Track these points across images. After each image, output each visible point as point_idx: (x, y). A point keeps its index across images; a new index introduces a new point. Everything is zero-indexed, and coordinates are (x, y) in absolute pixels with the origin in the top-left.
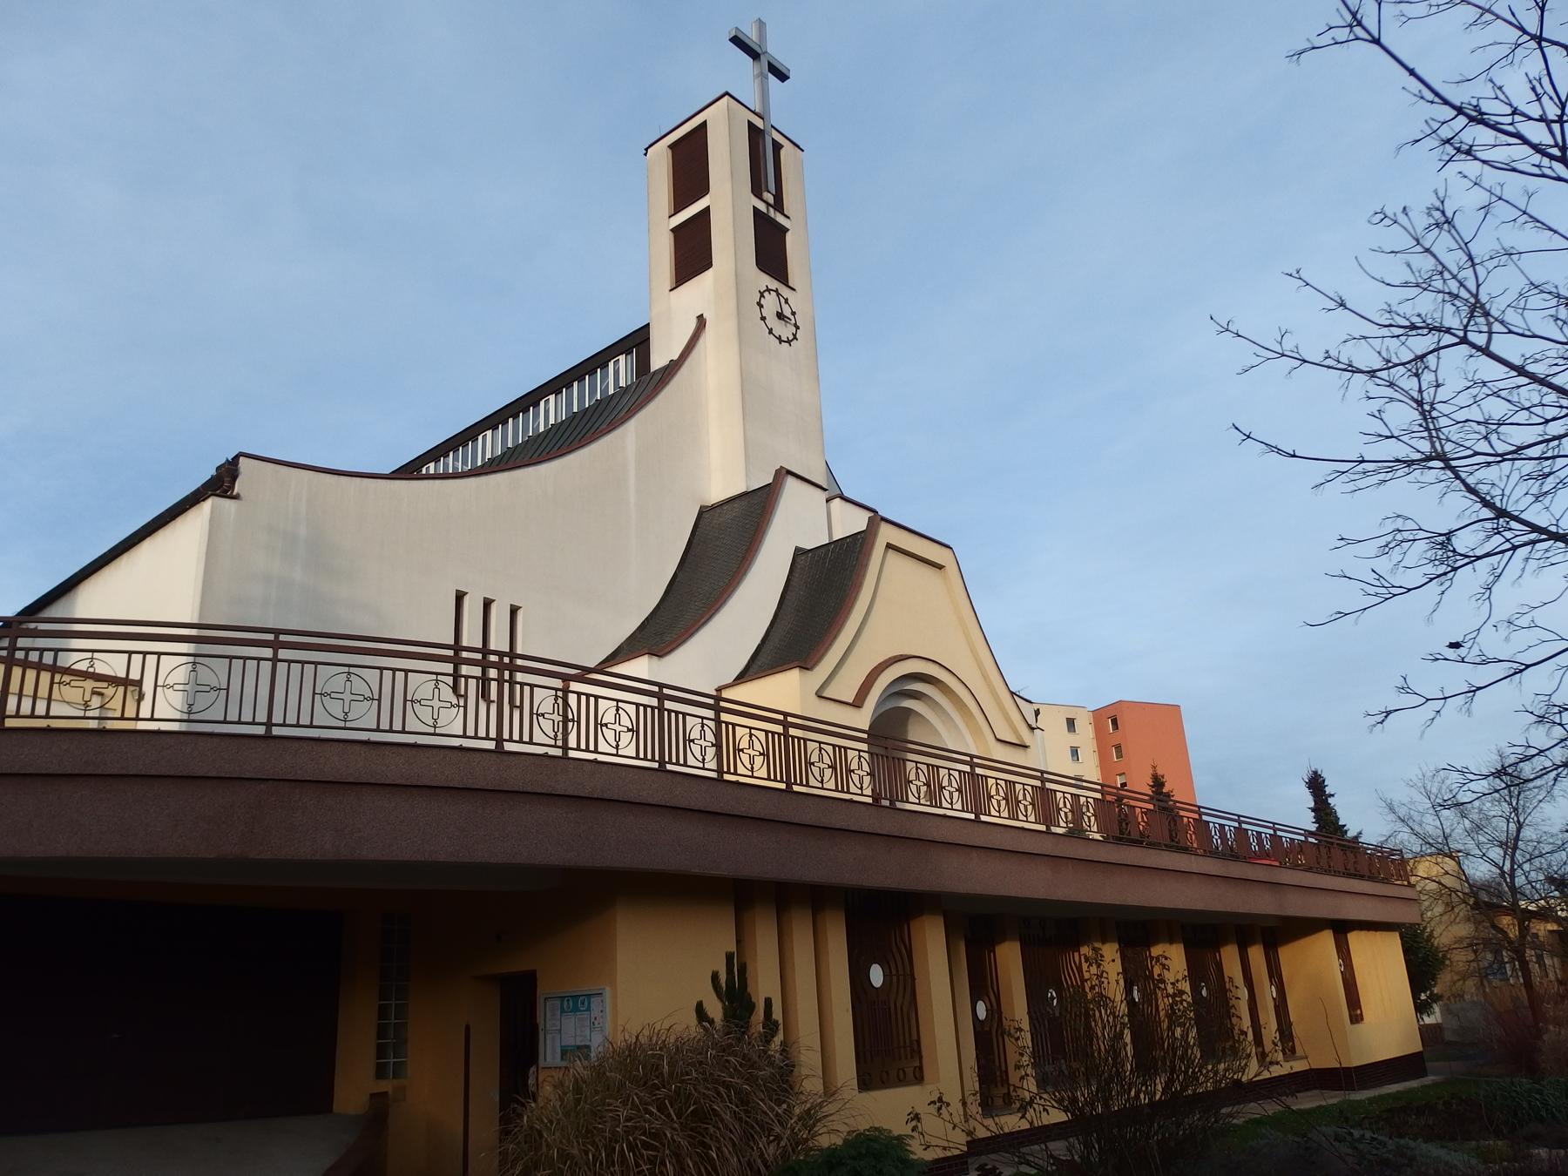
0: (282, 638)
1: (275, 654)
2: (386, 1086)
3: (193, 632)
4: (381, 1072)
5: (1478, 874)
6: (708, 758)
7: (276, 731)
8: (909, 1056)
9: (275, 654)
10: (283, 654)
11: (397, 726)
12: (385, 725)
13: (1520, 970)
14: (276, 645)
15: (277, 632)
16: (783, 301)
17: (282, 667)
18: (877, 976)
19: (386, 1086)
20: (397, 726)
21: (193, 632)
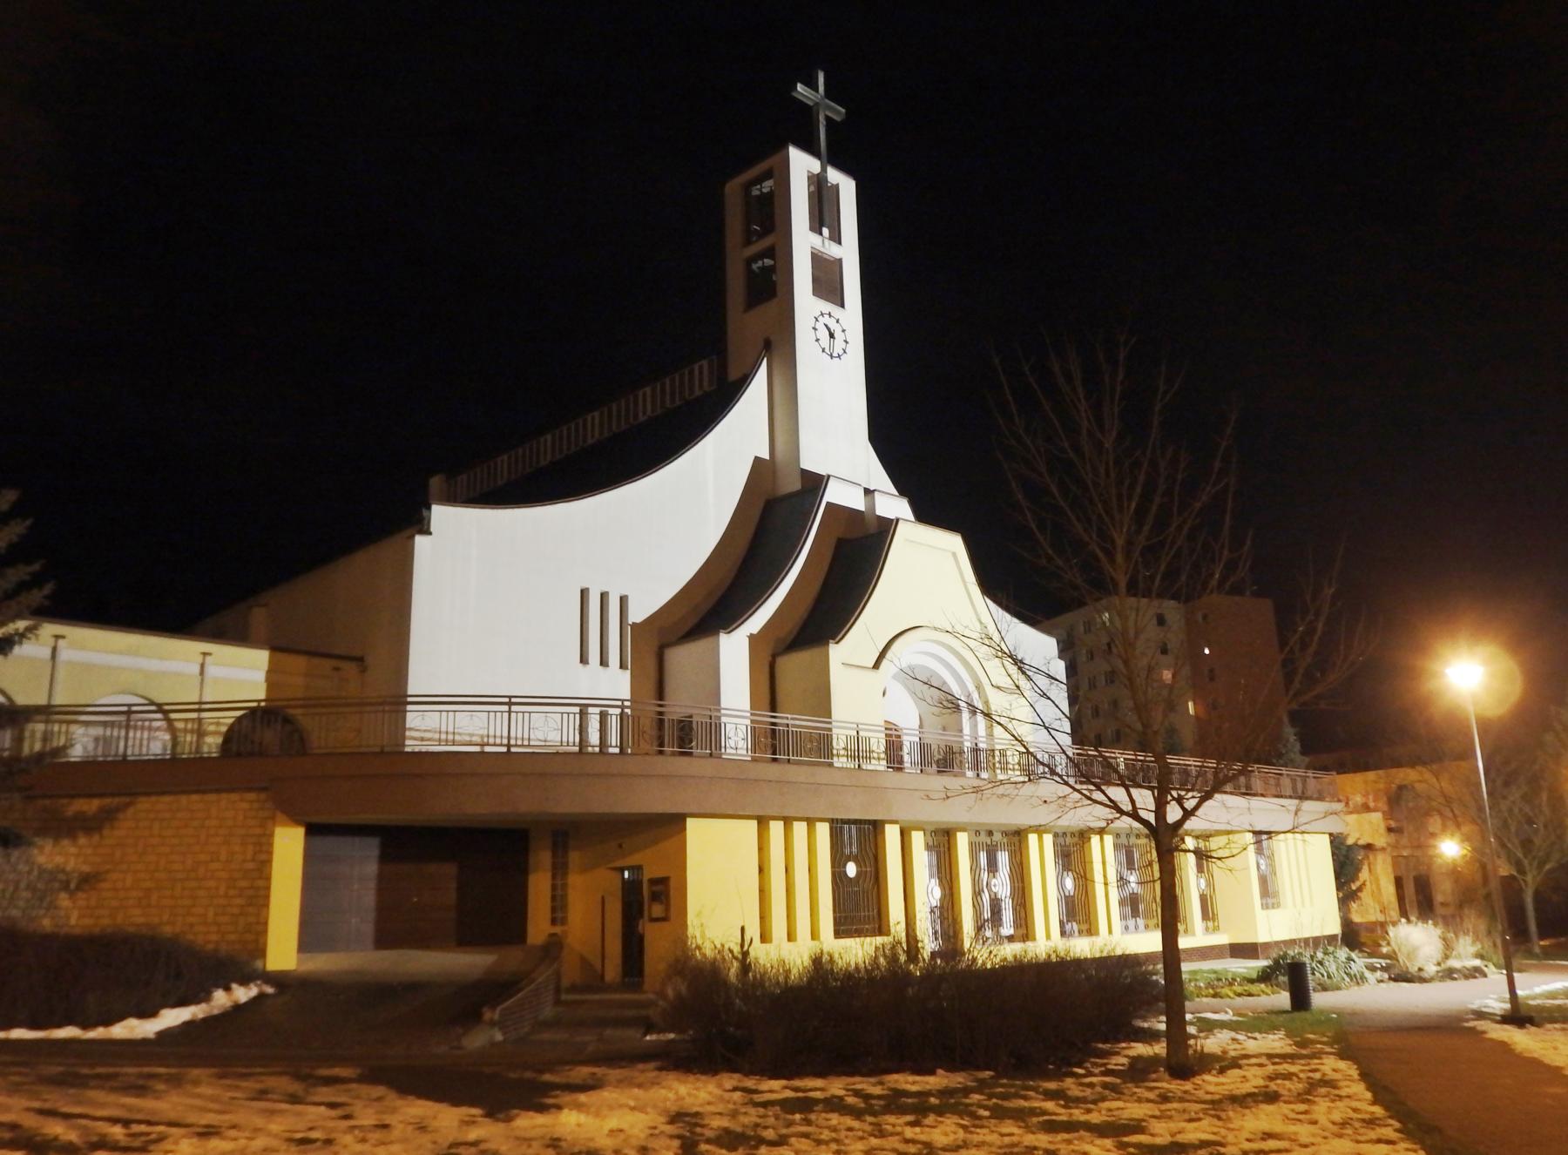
0: (513, 700)
1: (510, 708)
2: (558, 929)
3: (301, 702)
4: (554, 922)
5: (205, 1090)
6: (1106, 901)
7: (513, 750)
8: (888, 732)
9: (510, 708)
10: (514, 708)
11: (565, 716)
12: (527, 715)
13: (205, 997)
14: (510, 704)
15: (510, 697)
16: (827, 350)
17: (513, 715)
18: (851, 870)
19: (558, 929)
20: (565, 716)
21: (301, 702)
